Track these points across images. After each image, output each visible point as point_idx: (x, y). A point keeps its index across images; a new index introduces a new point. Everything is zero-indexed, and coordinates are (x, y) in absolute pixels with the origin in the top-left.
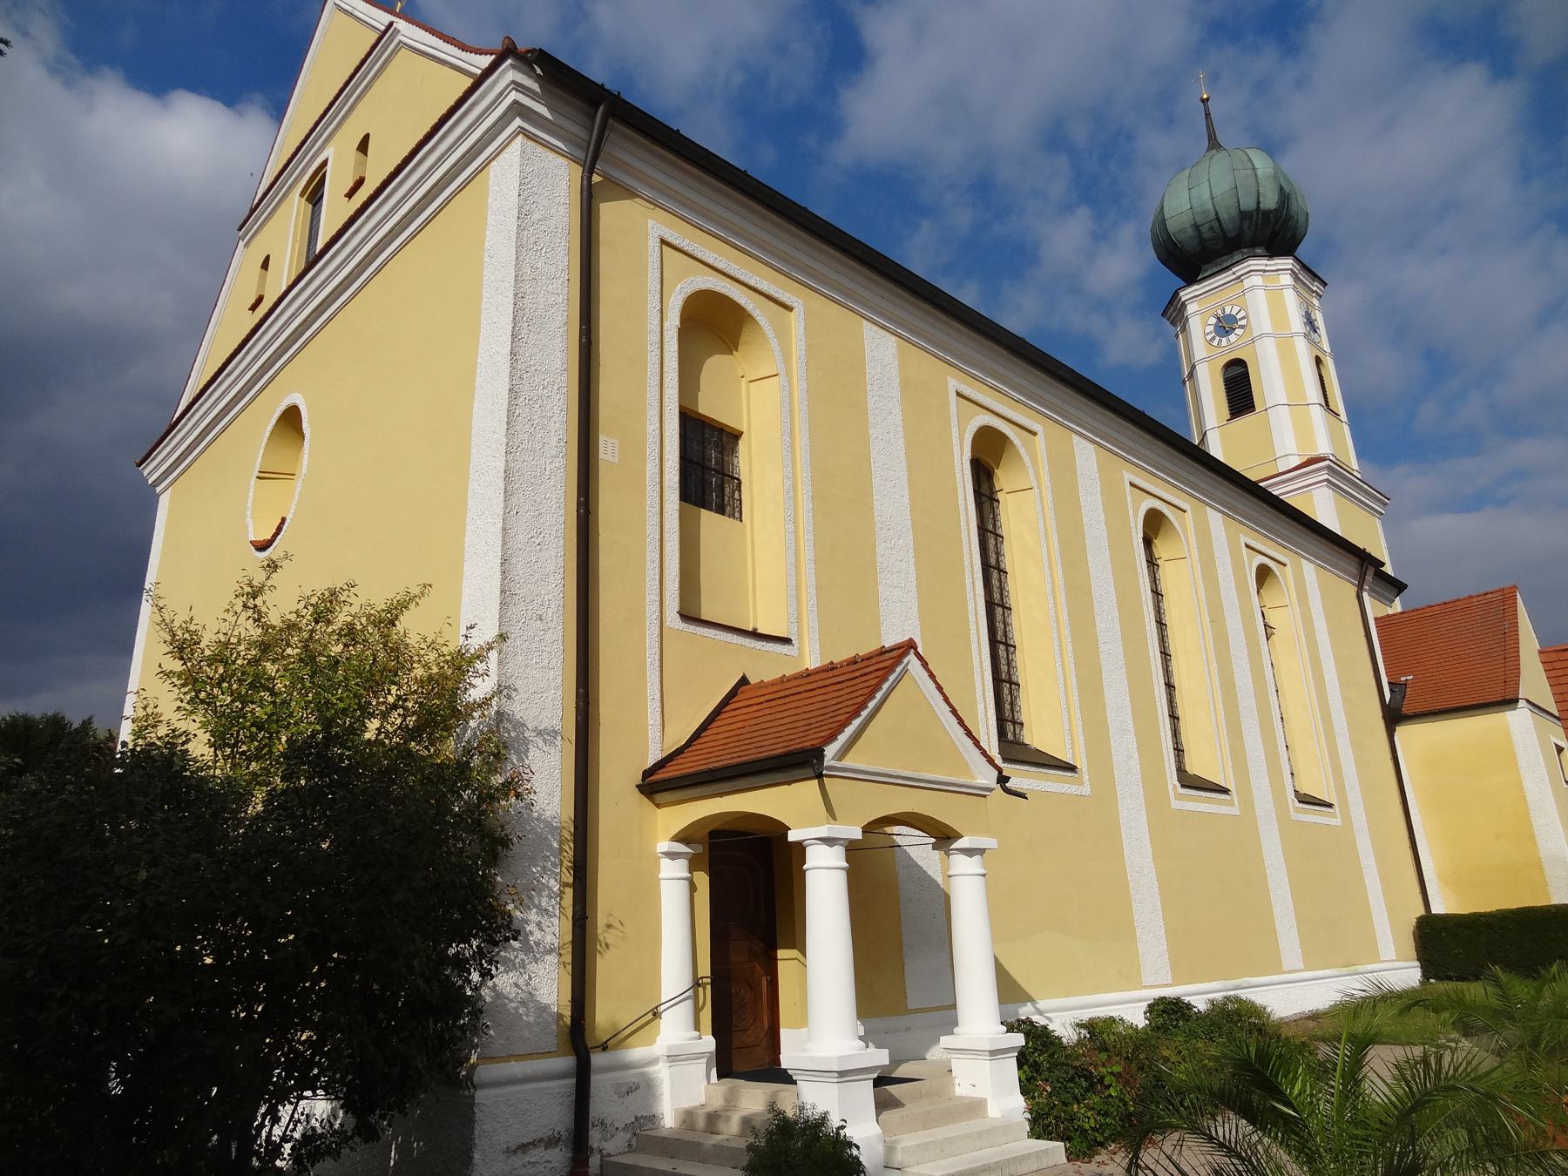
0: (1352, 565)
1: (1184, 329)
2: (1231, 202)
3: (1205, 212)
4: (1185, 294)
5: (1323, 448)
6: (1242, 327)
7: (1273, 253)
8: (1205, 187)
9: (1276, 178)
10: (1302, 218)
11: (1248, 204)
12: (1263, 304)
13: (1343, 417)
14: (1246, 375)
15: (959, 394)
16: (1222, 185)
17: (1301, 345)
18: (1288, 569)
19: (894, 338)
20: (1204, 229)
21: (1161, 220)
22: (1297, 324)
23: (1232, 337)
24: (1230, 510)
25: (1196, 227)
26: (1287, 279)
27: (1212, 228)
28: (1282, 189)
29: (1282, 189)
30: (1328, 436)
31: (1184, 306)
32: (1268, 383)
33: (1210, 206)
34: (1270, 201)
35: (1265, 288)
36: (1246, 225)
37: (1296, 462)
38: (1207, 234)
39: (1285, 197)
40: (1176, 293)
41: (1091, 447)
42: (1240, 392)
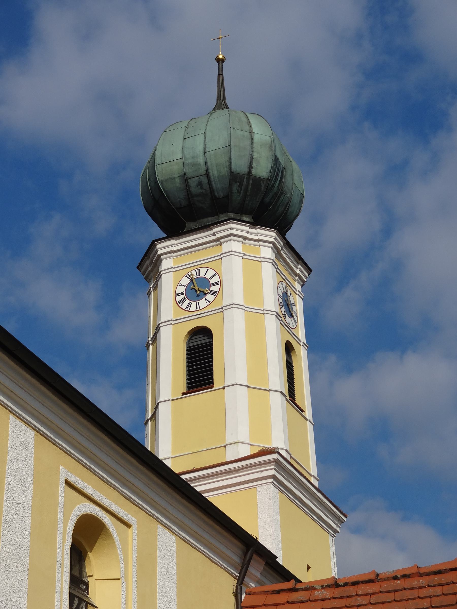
0: (234, 553)
1: (156, 287)
2: (223, 160)
3: (194, 165)
4: (161, 248)
5: (278, 441)
6: (214, 293)
7: (258, 221)
8: (199, 140)
9: (272, 147)
10: (295, 199)
11: (240, 165)
12: (239, 278)
13: (309, 414)
14: (210, 346)
15: (68, 483)
16: (217, 142)
17: (271, 325)
18: (132, 533)
19: (33, 433)
20: (193, 183)
21: (152, 165)
22: (271, 302)
23: (203, 303)
24: (48, 430)
25: (185, 178)
26: (267, 252)
27: (200, 184)
28: (276, 160)
29: (276, 160)
30: (285, 430)
31: (159, 261)
32: (231, 360)
33: (201, 160)
34: (262, 169)
35: (243, 256)
36: (235, 187)
37: (245, 451)
38: (195, 190)
39: (278, 170)
40: (153, 245)
41: (173, 538)
42: (200, 369)
